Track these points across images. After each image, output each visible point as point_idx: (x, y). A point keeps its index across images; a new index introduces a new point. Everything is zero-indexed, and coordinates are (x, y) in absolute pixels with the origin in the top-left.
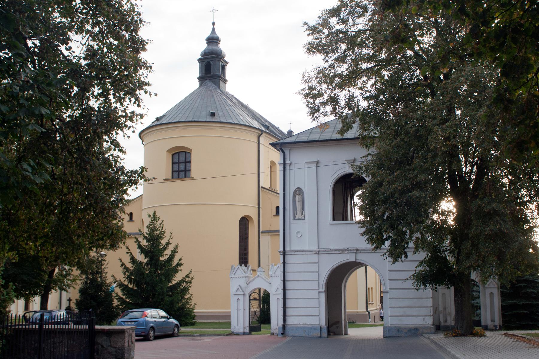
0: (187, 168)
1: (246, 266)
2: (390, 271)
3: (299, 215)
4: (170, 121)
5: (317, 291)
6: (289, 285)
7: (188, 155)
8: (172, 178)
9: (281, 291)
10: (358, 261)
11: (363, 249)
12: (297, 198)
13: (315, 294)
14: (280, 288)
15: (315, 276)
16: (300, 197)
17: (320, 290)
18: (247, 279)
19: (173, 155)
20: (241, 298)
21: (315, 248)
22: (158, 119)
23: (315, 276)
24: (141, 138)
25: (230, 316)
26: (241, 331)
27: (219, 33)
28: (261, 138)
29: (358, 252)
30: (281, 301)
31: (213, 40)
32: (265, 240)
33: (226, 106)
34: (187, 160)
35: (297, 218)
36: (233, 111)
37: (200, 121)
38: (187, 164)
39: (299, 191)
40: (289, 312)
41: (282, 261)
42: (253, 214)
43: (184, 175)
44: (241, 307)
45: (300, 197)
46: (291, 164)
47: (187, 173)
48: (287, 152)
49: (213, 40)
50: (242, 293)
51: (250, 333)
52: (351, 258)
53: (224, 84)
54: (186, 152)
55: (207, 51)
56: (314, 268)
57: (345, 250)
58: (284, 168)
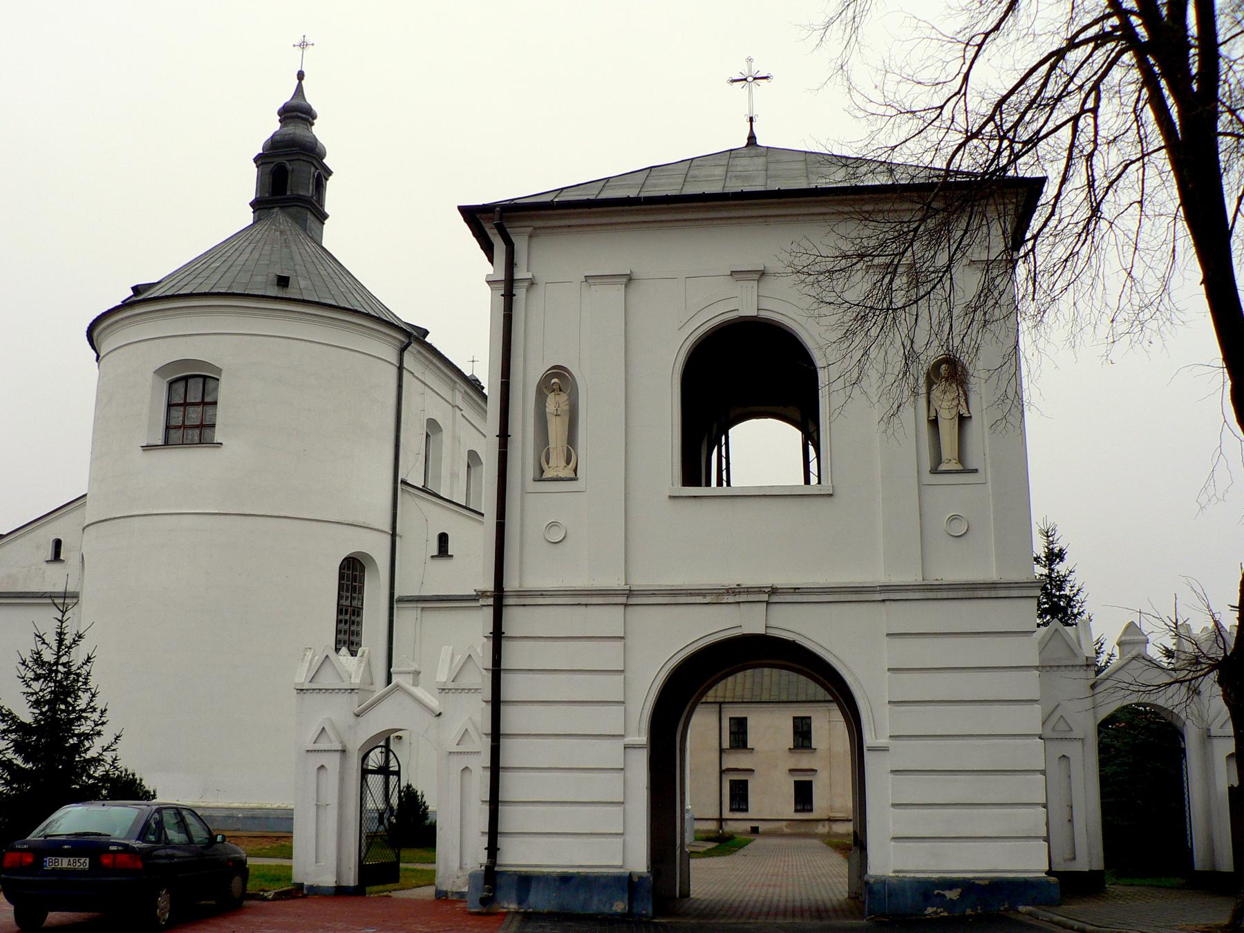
1: (353, 654)
3: (557, 467)
4: (169, 293)
5: (620, 744)
6: (512, 719)
7: (210, 384)
11: (796, 590)
12: (552, 402)
16: (563, 398)
17: (630, 740)
18: (355, 698)
19: (171, 384)
20: (333, 762)
22: (137, 290)
24: (94, 348)
25: (289, 837)
26: (329, 880)
27: (312, 99)
28: (406, 354)
29: (775, 599)
31: (297, 113)
33: (319, 267)
35: (547, 474)
36: (337, 281)
39: (558, 380)
40: (510, 819)
42: (378, 550)
43: (196, 439)
46: (532, 283)
47: (207, 431)
48: (520, 243)
49: (297, 113)
53: (317, 223)
54: (205, 377)
55: (277, 138)
56: (610, 655)
58: (509, 296)
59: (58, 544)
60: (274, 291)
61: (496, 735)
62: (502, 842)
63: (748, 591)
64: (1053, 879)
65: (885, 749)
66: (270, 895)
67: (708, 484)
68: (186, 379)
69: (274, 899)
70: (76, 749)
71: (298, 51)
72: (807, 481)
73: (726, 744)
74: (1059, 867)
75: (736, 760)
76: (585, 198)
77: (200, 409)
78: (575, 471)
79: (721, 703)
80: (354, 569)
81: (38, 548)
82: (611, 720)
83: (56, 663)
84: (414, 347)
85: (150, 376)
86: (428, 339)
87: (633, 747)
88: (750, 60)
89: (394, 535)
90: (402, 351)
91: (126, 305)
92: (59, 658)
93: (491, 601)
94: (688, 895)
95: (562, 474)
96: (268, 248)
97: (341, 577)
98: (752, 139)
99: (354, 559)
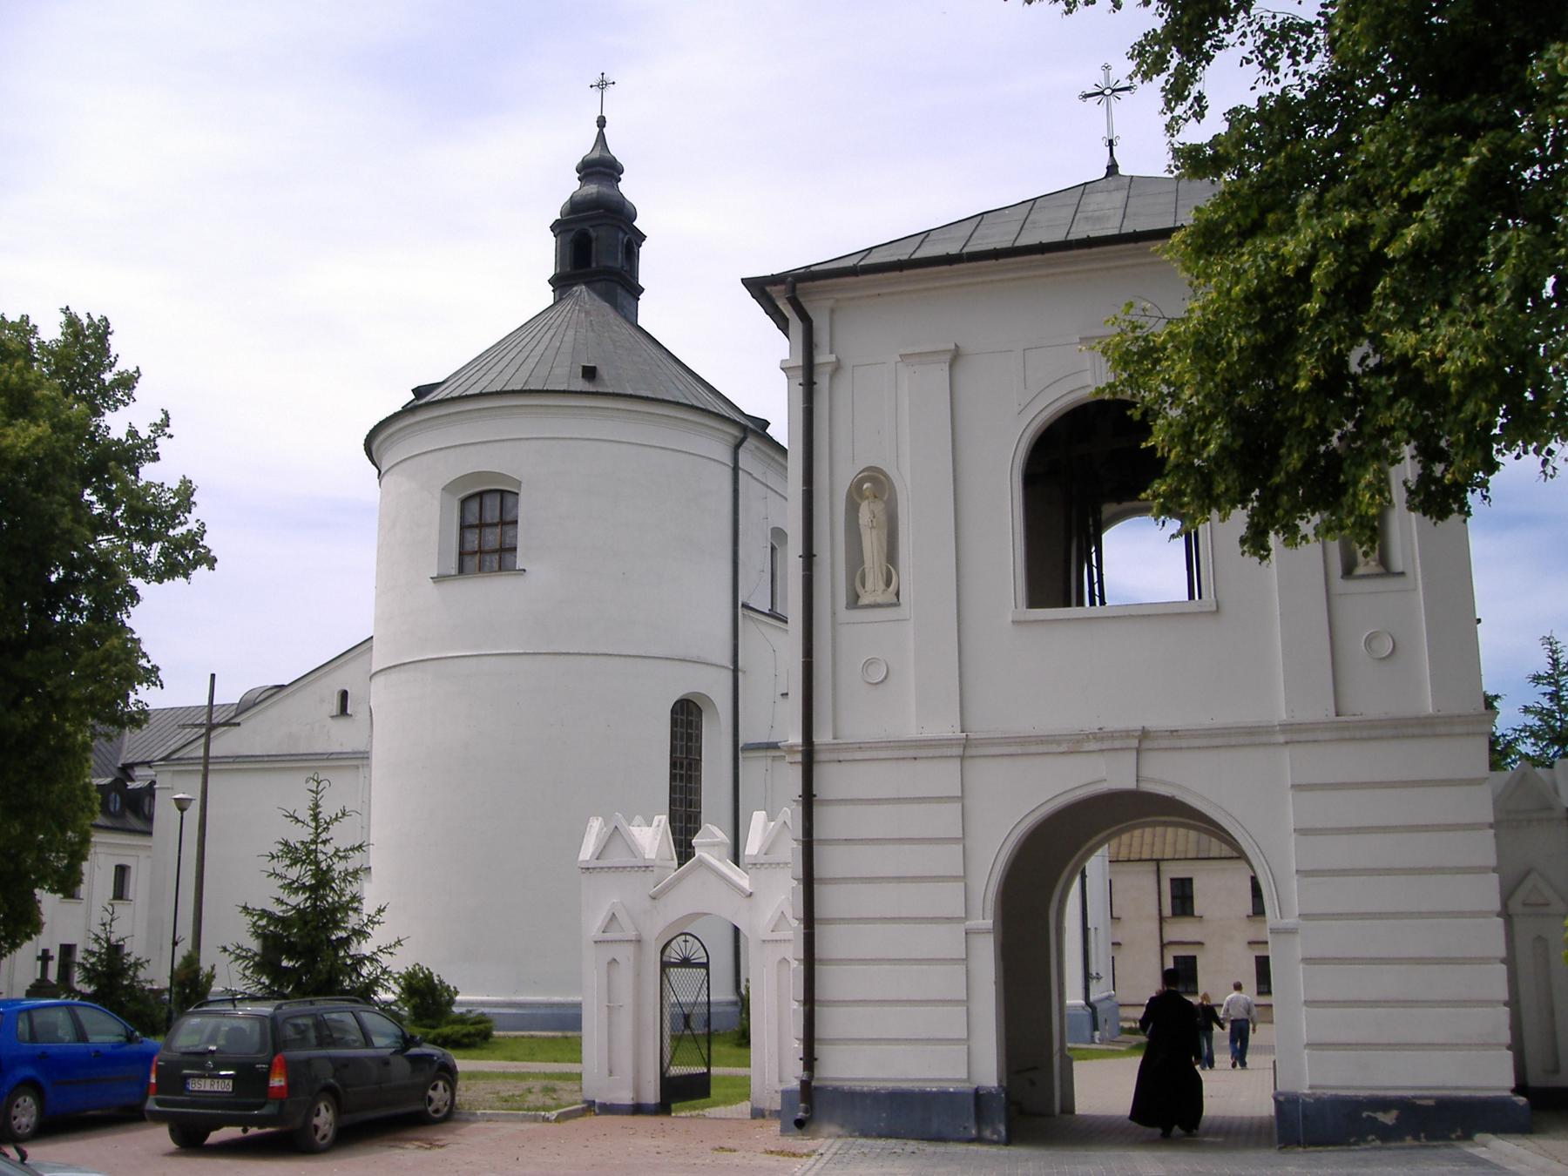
0: (508, 542)
2: (1301, 832)
3: (873, 591)
4: (455, 394)
5: (960, 930)
6: (829, 901)
7: (509, 500)
8: (461, 570)
9: (795, 929)
10: (1147, 787)
13: (948, 941)
14: (789, 915)
15: (947, 860)
16: (879, 507)
17: (971, 924)
19: (464, 502)
20: (625, 954)
21: (947, 727)
22: (419, 392)
23: (947, 860)
26: (625, 1097)
27: (616, 149)
28: (741, 451)
30: (797, 967)
31: (600, 168)
32: (752, 769)
34: (509, 518)
35: (864, 601)
37: (547, 391)
38: (507, 528)
40: (830, 1022)
41: (798, 789)
42: (717, 689)
43: (496, 566)
44: (626, 997)
45: (879, 507)
46: (837, 367)
47: (508, 557)
49: (600, 168)
50: (632, 935)
51: (663, 1108)
52: (1116, 775)
53: (631, 299)
54: (502, 492)
56: (946, 820)
57: (1088, 737)
58: (809, 385)
59: (344, 695)
60: (580, 384)
61: (809, 919)
62: (820, 1050)
63: (1112, 735)
64: (1522, 1100)
65: (1291, 931)
66: (554, 1114)
67: (1080, 603)
68: (481, 494)
69: (557, 1120)
70: (345, 942)
71: (596, 93)
72: (1191, 596)
73: (1167, 911)
74: (1535, 1080)
75: (1180, 930)
76: (895, 258)
77: (498, 530)
78: (897, 594)
79: (1158, 861)
80: (689, 713)
81: (322, 701)
83: (314, 842)
84: (751, 442)
85: (438, 493)
86: (205, 567)
87: (979, 932)
88: (1107, 68)
89: (736, 670)
90: (737, 448)
91: (408, 410)
92: (318, 835)
93: (799, 758)
94: (1072, 1111)
95: (880, 600)
96: (571, 333)
97: (674, 723)
98: (1112, 169)
99: (688, 701)
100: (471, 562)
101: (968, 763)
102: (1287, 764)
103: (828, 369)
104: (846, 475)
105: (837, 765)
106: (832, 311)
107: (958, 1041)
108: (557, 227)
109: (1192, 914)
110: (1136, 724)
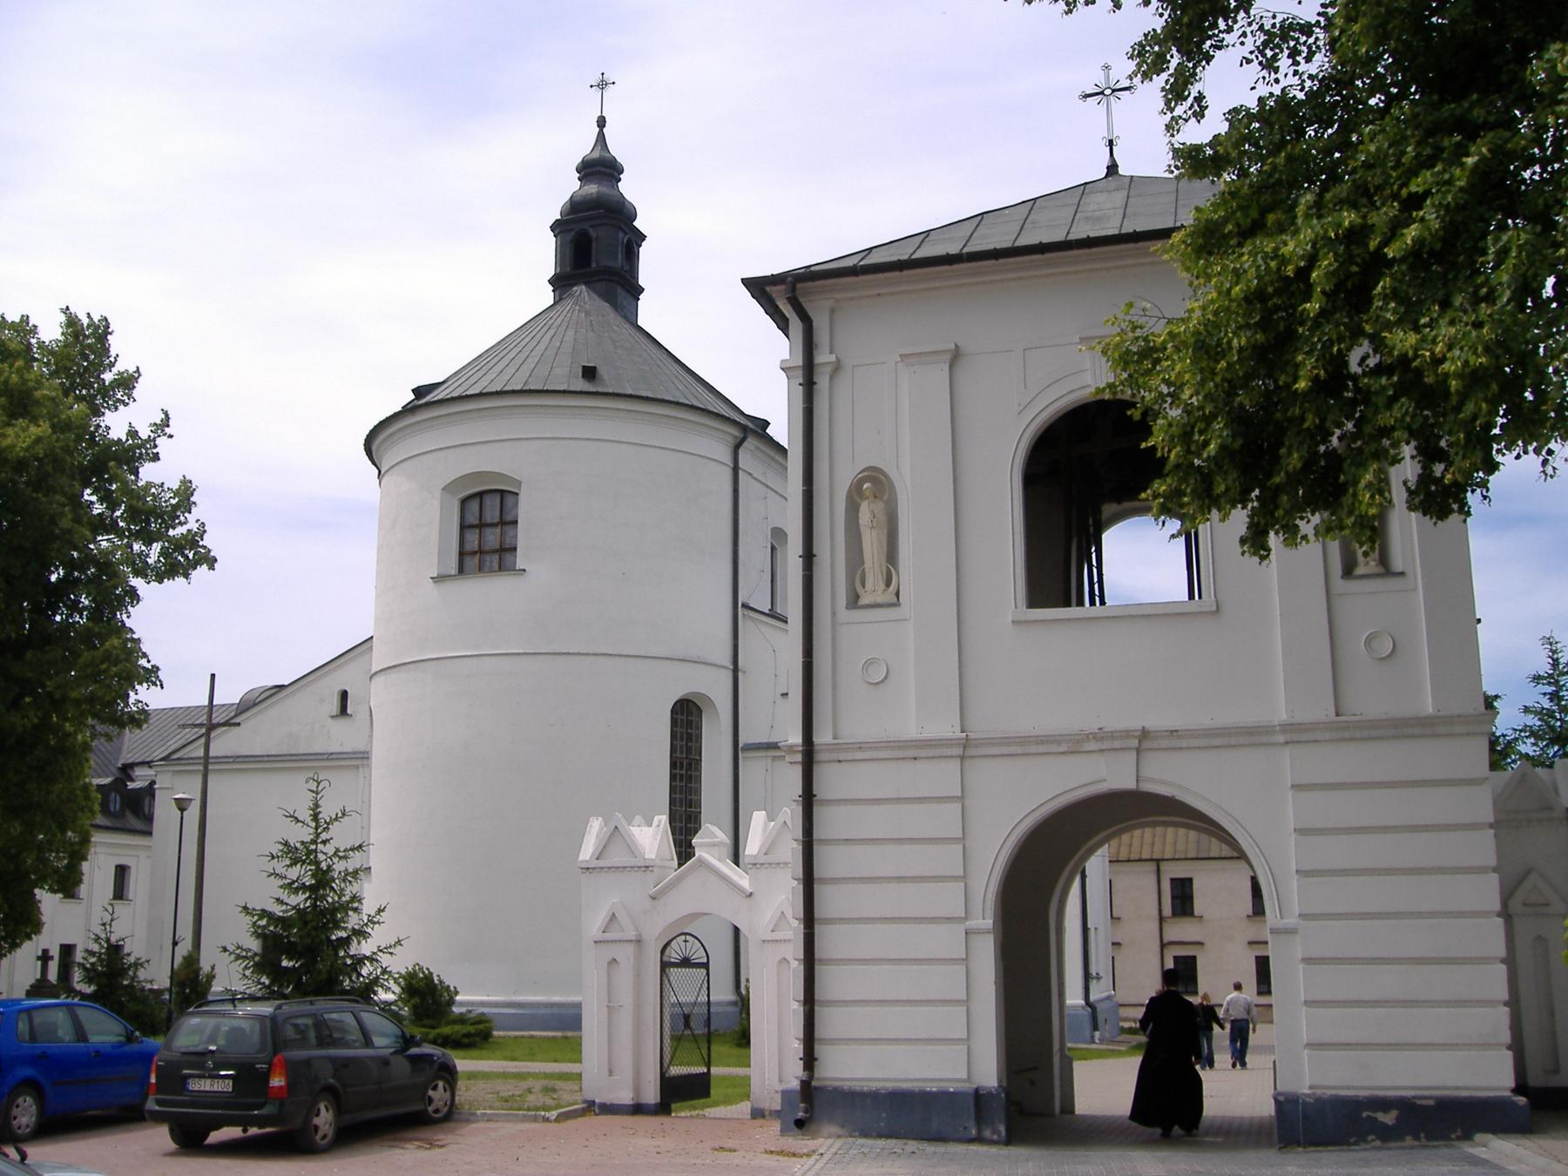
0: (508, 542)
2: (1301, 832)
3: (873, 591)
4: (455, 394)
5: (960, 930)
6: (829, 901)
7: (509, 500)
8: (461, 570)
9: (795, 929)
10: (1147, 787)
13: (948, 941)
14: (789, 915)
15: (947, 860)
16: (879, 507)
17: (971, 924)
19: (464, 502)
20: (625, 954)
21: (947, 727)
22: (419, 392)
23: (947, 860)
26: (625, 1097)
27: (616, 149)
28: (741, 451)
30: (797, 967)
31: (600, 168)
32: (752, 769)
34: (509, 518)
35: (864, 601)
37: (547, 391)
38: (507, 528)
40: (830, 1022)
41: (798, 789)
42: (717, 689)
43: (496, 566)
44: (626, 997)
45: (879, 507)
46: (837, 367)
47: (508, 557)
49: (600, 168)
50: (632, 935)
51: (663, 1108)
52: (1116, 775)
53: (631, 299)
54: (502, 492)
56: (946, 820)
57: (1088, 737)
58: (809, 385)
59: (344, 695)
60: (580, 384)
61: (809, 919)
62: (820, 1050)
63: (1112, 735)
64: (1522, 1100)
65: (1291, 931)
66: (554, 1114)
67: (1080, 603)
68: (481, 494)
69: (557, 1120)
70: (345, 942)
71: (596, 93)
72: (1191, 596)
73: (1167, 911)
74: (1535, 1080)
75: (1180, 930)
76: (895, 258)
77: (498, 530)
78: (897, 594)
79: (1158, 861)
80: (689, 713)
81: (322, 701)
82: (949, 899)
83: (314, 842)
84: (751, 442)
85: (438, 493)
87: (979, 932)
88: (1107, 68)
89: (736, 670)
90: (737, 448)
91: (408, 410)
92: (318, 835)
93: (799, 758)
94: (1072, 1111)
95: (880, 600)
96: (571, 333)
97: (674, 723)
98: (1112, 169)
99: (688, 701)
100: (471, 562)
101: (968, 763)
102: (1287, 764)
103: (828, 369)
104: (846, 475)
105: (837, 765)
106: (832, 311)
107: (958, 1041)
108: (557, 227)
109: (1192, 914)
110: (1136, 724)
